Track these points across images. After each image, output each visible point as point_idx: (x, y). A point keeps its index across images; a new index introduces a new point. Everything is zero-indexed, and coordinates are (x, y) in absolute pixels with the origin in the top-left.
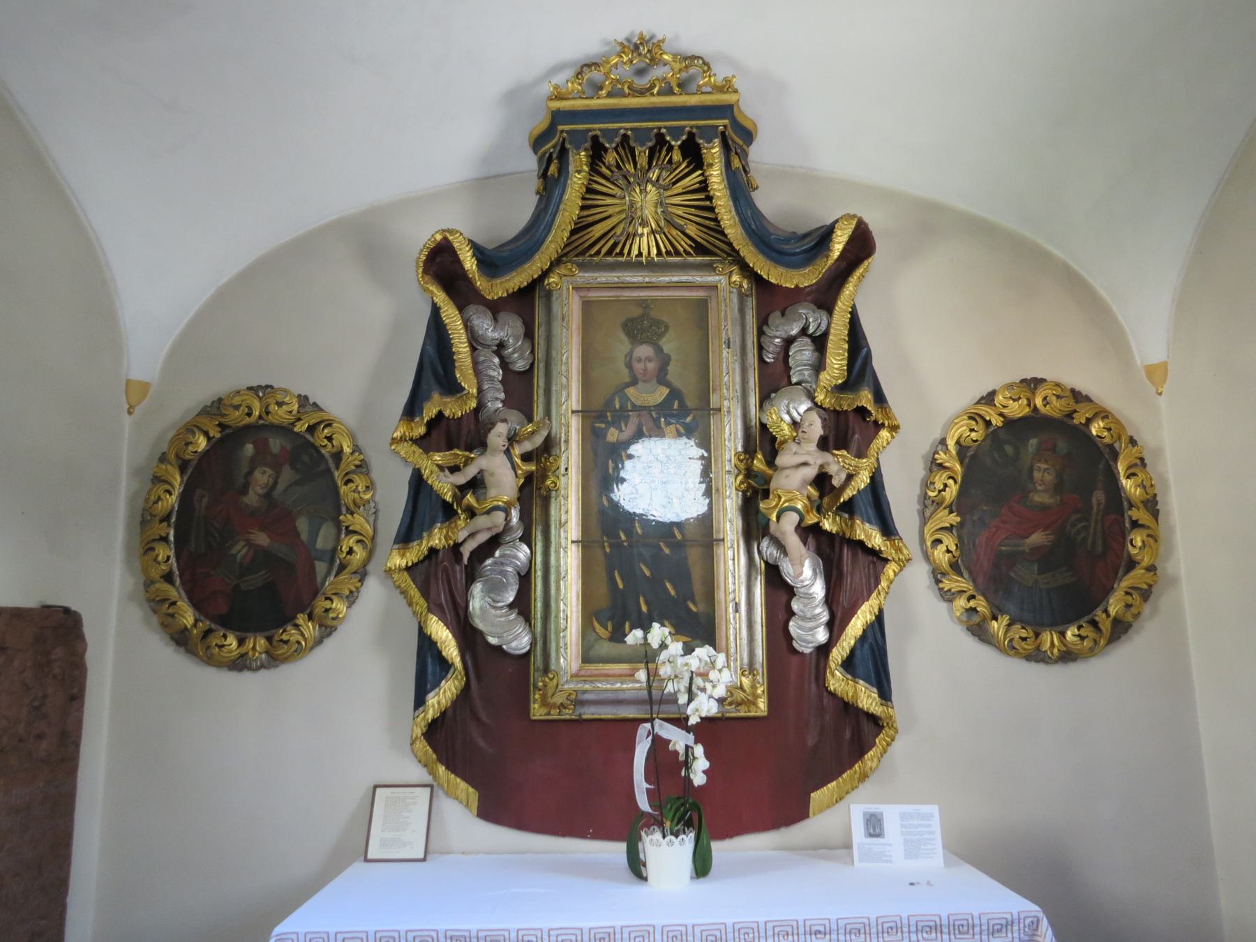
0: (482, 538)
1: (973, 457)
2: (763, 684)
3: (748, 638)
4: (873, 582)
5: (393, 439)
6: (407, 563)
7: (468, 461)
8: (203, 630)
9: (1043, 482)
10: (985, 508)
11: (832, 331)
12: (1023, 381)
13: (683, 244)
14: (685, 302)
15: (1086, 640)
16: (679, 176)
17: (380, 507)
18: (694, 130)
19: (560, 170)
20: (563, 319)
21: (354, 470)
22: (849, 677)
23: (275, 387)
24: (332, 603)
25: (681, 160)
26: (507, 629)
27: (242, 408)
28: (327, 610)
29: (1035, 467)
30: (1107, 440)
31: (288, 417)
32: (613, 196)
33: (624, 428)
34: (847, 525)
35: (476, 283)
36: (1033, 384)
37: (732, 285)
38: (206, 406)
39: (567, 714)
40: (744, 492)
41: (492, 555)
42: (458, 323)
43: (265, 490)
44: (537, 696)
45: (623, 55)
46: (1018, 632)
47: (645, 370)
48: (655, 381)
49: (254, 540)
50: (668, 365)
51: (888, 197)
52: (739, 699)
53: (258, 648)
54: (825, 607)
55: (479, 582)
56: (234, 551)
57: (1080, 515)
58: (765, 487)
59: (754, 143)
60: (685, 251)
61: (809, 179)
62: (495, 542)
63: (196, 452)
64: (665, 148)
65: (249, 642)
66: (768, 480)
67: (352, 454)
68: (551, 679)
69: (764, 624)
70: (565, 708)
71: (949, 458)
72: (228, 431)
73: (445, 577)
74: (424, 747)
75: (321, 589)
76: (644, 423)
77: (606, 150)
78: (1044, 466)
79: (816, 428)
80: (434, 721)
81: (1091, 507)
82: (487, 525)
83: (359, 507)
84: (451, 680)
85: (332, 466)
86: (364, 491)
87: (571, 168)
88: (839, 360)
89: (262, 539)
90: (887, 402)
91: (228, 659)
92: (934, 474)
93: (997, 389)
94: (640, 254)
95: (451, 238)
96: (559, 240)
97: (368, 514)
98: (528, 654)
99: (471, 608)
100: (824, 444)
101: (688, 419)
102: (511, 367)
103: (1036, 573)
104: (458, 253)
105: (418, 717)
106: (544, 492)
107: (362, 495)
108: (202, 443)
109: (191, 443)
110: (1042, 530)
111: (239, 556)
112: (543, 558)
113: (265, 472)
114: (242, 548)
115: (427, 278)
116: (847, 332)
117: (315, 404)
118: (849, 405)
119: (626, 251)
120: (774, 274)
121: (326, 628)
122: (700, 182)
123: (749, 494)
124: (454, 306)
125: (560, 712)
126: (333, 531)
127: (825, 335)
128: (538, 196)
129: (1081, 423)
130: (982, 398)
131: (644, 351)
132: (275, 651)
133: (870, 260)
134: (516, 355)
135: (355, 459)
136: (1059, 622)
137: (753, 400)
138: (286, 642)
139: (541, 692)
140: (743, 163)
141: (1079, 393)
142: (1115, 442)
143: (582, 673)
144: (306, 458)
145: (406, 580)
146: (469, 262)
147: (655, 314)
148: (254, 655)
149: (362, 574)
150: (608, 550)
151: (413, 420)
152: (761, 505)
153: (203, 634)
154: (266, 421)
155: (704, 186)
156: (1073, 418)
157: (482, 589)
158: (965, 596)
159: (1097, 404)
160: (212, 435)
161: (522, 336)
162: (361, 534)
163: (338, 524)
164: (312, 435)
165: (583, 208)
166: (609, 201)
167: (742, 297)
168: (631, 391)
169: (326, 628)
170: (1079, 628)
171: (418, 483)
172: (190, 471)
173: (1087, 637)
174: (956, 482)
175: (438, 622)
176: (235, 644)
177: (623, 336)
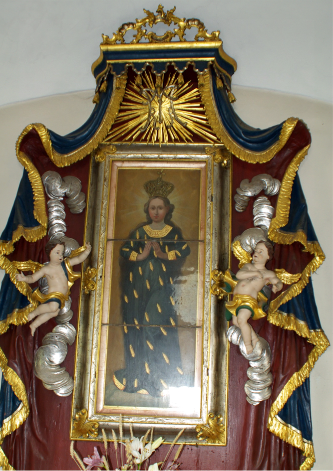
0: (44, 319)
7: (38, 268)
11: (282, 193)
13: (186, 135)
16: (182, 92)
18: (193, 64)
20: (105, 180)
25: (183, 82)
32: (141, 104)
33: (141, 252)
34: (286, 320)
47: (157, 214)
48: (163, 222)
51: (323, 108)
58: (231, 293)
59: (235, 73)
60: (187, 139)
62: (53, 323)
64: (175, 75)
77: (136, 75)
79: (263, 253)
80: (7, 436)
82: (48, 311)
88: (284, 211)
94: (158, 140)
95: (37, 129)
96: (105, 130)
100: (270, 265)
101: (184, 248)
102: (71, 210)
115: (21, 153)
116: (290, 193)
119: (148, 138)
122: (197, 96)
124: (37, 171)
128: (95, 104)
131: (157, 202)
140: (225, 84)
152: (226, 305)
161: (79, 191)
166: (139, 107)
168: (147, 228)
177: (144, 192)
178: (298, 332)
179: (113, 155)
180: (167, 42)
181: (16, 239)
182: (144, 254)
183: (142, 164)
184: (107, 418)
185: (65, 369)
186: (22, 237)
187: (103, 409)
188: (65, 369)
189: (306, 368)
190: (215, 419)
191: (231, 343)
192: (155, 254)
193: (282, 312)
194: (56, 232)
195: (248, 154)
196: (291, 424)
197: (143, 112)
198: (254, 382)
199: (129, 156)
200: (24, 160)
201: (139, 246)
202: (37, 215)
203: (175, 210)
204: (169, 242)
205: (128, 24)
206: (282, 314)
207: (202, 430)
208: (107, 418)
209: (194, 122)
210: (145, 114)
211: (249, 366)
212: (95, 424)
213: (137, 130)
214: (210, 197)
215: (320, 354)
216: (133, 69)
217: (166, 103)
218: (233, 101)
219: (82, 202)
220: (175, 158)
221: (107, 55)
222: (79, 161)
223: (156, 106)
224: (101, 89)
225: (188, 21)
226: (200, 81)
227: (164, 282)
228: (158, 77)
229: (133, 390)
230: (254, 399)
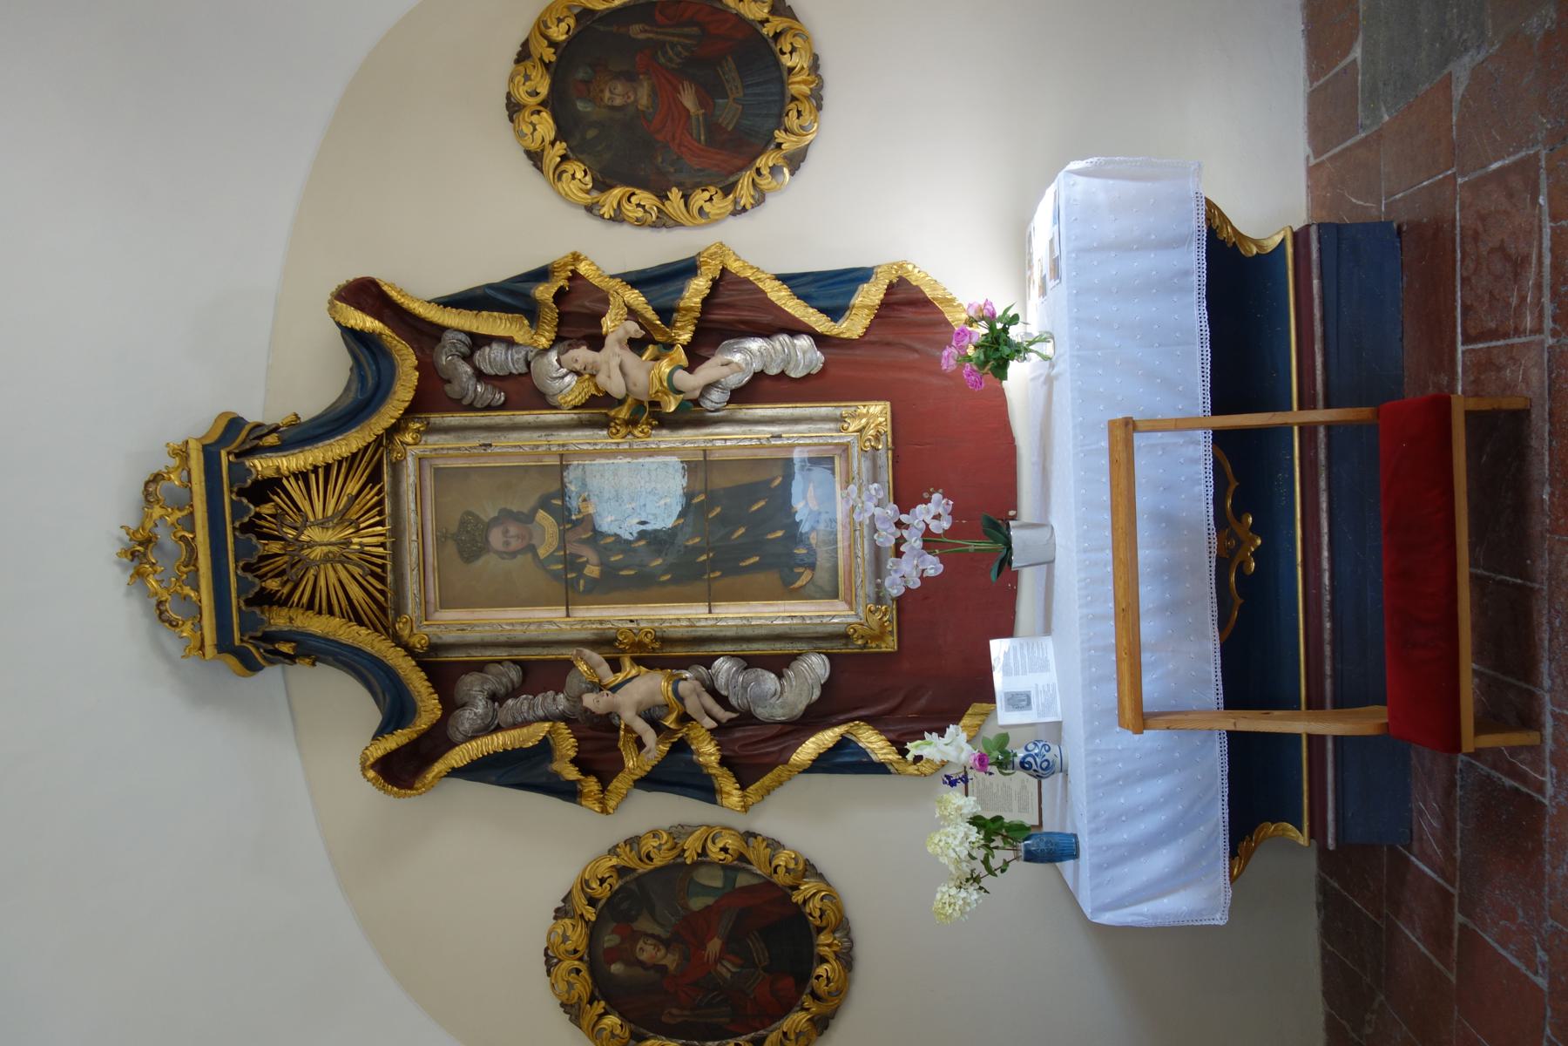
6: (736, 789)
13: (370, 497)
20: (463, 630)
23: (546, 946)
24: (780, 865)
28: (788, 870)
29: (609, 104)
33: (585, 559)
38: (570, 1019)
44: (874, 645)
47: (518, 537)
53: (829, 942)
56: (728, 976)
57: (659, 53)
63: (621, 1026)
67: (618, 856)
68: (855, 631)
69: (794, 405)
78: (607, 94)
81: (649, 39)
83: (676, 844)
86: (659, 839)
89: (714, 946)
90: (547, 266)
91: (842, 973)
103: (726, 100)
107: (663, 842)
108: (612, 1020)
109: (612, 1032)
111: (734, 970)
113: (641, 949)
114: (724, 966)
117: (564, 900)
119: (380, 561)
120: (404, 392)
121: (806, 870)
126: (703, 870)
131: (496, 538)
137: (549, 417)
138: (822, 912)
147: (454, 528)
148: (837, 945)
149: (749, 835)
155: (302, 476)
158: (758, 180)
165: (331, 612)
168: (543, 552)
173: (791, 44)
177: (480, 562)
201: (572, 564)
203: (509, 507)
212: (870, 611)
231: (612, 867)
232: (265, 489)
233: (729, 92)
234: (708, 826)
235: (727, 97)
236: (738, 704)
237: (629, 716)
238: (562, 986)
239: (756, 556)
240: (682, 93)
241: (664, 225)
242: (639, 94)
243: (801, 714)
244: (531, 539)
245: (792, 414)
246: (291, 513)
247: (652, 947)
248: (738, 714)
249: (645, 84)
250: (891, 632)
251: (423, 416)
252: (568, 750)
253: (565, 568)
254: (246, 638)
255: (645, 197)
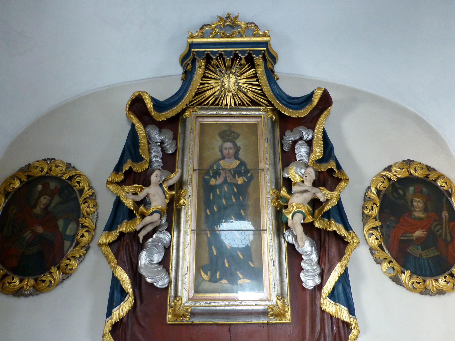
1: (385, 195)
2: (288, 306)
3: (280, 279)
4: (341, 255)
5: (108, 181)
6: (109, 241)
8: (2, 274)
9: (418, 207)
10: (392, 219)
11: (315, 137)
12: (404, 161)
13: (246, 100)
14: (247, 125)
15: (449, 284)
16: (244, 71)
17: (99, 215)
18: (251, 52)
19: (192, 68)
20: (191, 129)
21: (89, 197)
22: (333, 302)
23: (56, 159)
24: (70, 261)
26: (157, 275)
27: (39, 168)
28: (67, 265)
29: (414, 200)
30: (446, 188)
31: (60, 173)
33: (218, 179)
34: (327, 224)
35: (152, 113)
36: (409, 163)
37: (268, 116)
38: (22, 167)
39: (186, 321)
40: (276, 208)
41: (152, 237)
42: (143, 131)
43: (45, 206)
44: (171, 311)
45: (221, 22)
46: (415, 280)
47: (229, 153)
49: (36, 230)
50: (239, 151)
51: (337, 86)
52: (276, 312)
53: (29, 284)
54: (318, 266)
55: (145, 250)
56: (25, 235)
57: (437, 223)
60: (247, 103)
61: (301, 80)
63: (14, 188)
65: (25, 281)
66: (287, 201)
67: (88, 190)
68: (178, 301)
69: (287, 274)
70: (185, 317)
71: (373, 194)
72: (31, 179)
73: (127, 247)
74: (110, 339)
75: (66, 254)
76: (227, 176)
77: (212, 59)
78: (418, 200)
80: (115, 323)
81: (443, 219)
83: (89, 215)
84: (127, 302)
85: (78, 195)
86: (93, 207)
87: (197, 67)
89: (40, 230)
90: (342, 169)
91: (12, 290)
92: (366, 202)
93: (392, 165)
97: (93, 218)
98: (167, 288)
99: (139, 264)
100: (315, 184)
101: (249, 175)
102: (166, 152)
103: (420, 250)
104: (145, 100)
105: (108, 321)
106: (179, 207)
107: (91, 209)
108: (17, 184)
109: (12, 184)
110: (420, 229)
111: (27, 238)
112: (177, 240)
113: (46, 198)
114: (29, 234)
116: (322, 137)
117: (74, 167)
118: (325, 169)
119: (220, 103)
120: (287, 112)
121: (66, 274)
122: (254, 74)
123: (278, 209)
124: (141, 124)
125: (182, 319)
126: (75, 226)
127: (311, 140)
129: (432, 180)
130: (386, 168)
131: (228, 145)
132: (38, 286)
133: (330, 108)
134: (169, 146)
135: (90, 192)
136: (435, 274)
137: (279, 166)
138: (44, 281)
139: (172, 308)
141: (430, 167)
142: (449, 189)
143: (194, 298)
144: (66, 192)
145: (108, 250)
146: (150, 105)
147: (234, 130)
148: (26, 288)
149: (87, 248)
150: (209, 236)
151: (118, 174)
153: (2, 276)
154: (50, 174)
155: (255, 76)
156: (429, 178)
157: (145, 254)
158: (387, 261)
159: (438, 172)
160: (22, 180)
162: (89, 228)
163: (78, 222)
164: (71, 181)
165: (201, 84)
167: (273, 123)
168: (222, 162)
169: (66, 274)
170: (445, 277)
171: (118, 203)
172: (10, 197)
173: (450, 282)
174: (377, 206)
175: (121, 270)
176: (18, 282)
177: (218, 138)
178: (338, 232)
179: (196, 113)
180: (233, 37)
181: (126, 169)
182: (220, 181)
183: (217, 120)
184: (197, 303)
185: (162, 266)
186: (130, 167)
187: (194, 296)
188: (162, 266)
189: (345, 259)
190: (282, 300)
191: (288, 243)
192: (228, 180)
193: (324, 218)
194: (155, 166)
195: (291, 112)
196: (339, 302)
197: (217, 85)
198: (307, 271)
199: (208, 113)
200: (132, 116)
201: (216, 174)
202: (142, 152)
203: (241, 150)
204: (237, 172)
205: (206, 25)
206: (324, 220)
207: (273, 310)
208: (197, 304)
209: (252, 91)
210: (217, 86)
211: (303, 259)
212: (188, 309)
213: (212, 97)
214: (266, 140)
215: (353, 250)
216: (210, 55)
217: (233, 79)
218: (278, 79)
219: (174, 145)
220: (240, 114)
221: (192, 45)
222: (172, 117)
223: (226, 81)
224: (188, 68)
225: (247, 24)
226: (256, 62)
227: (236, 199)
228: (227, 60)
229: (216, 281)
230: (308, 284)
231: (84, 187)
232: (250, 61)
233: (424, 252)
234: (95, 229)
235: (422, 250)
236: (149, 243)
237: (147, 190)
238: (37, 164)
239: (217, 253)
240: (421, 231)
241: (363, 218)
242: (419, 213)
243: (141, 273)
244: (228, 158)
245: (283, 272)
246: (241, 71)
247: (45, 203)
248: (141, 242)
249: (423, 216)
250: (176, 320)
251: (278, 120)
252: (136, 169)
253: (214, 170)
254: (195, 53)
255: (375, 211)
